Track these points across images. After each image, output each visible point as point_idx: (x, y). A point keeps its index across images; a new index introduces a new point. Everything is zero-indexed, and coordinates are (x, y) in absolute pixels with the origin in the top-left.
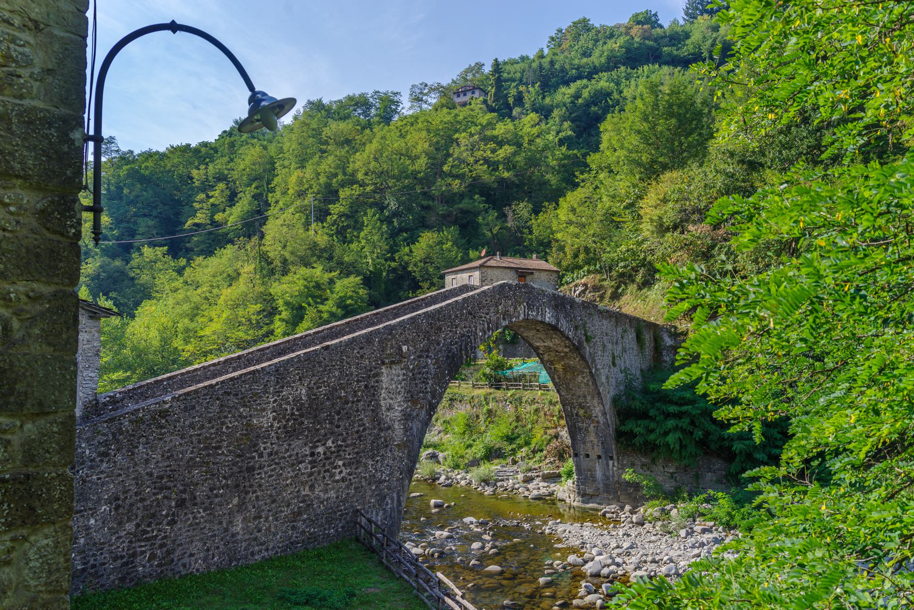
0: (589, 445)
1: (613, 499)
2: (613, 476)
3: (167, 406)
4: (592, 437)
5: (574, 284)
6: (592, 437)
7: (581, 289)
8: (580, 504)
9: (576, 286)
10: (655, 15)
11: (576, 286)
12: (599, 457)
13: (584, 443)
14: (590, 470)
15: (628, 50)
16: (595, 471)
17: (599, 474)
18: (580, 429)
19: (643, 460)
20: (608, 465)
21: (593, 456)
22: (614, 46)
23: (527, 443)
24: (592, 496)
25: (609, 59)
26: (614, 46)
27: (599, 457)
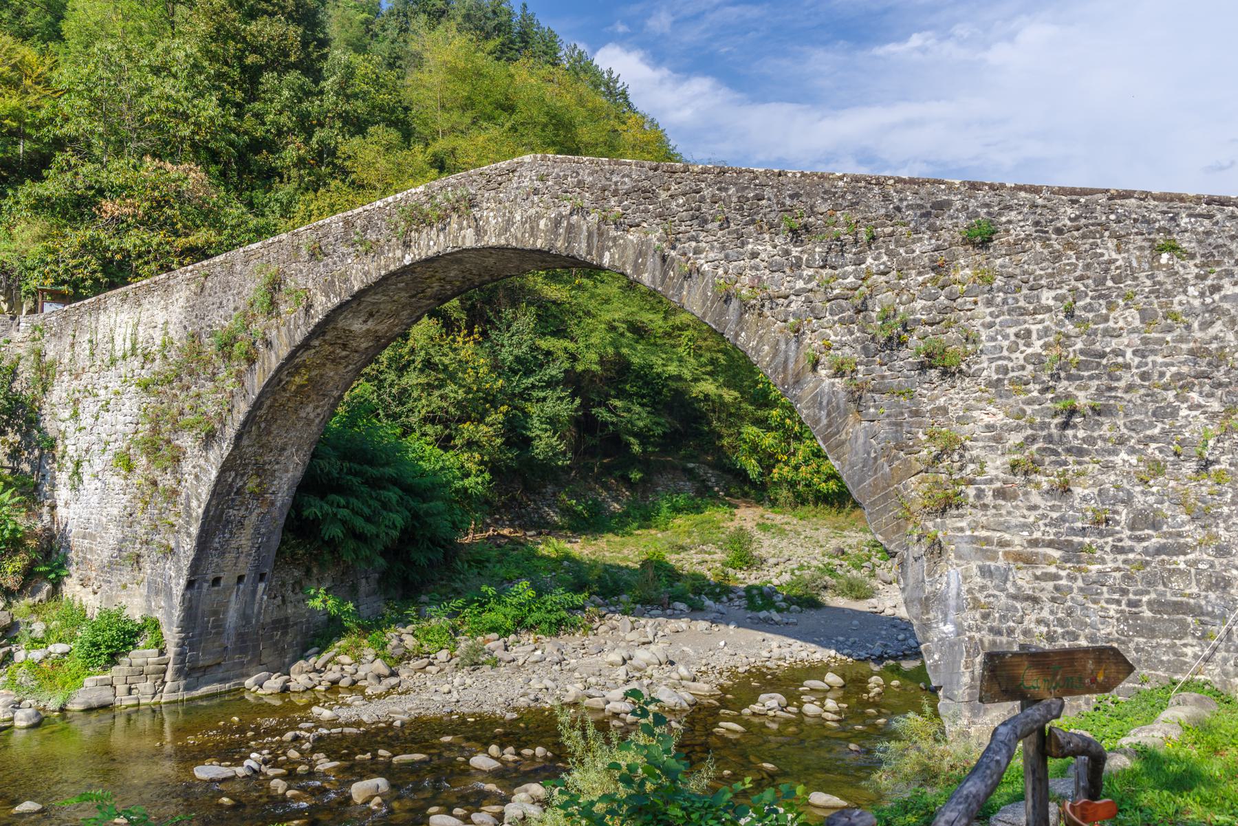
1: (250, 662)
3: (344, 353)
4: (244, 539)
6: (244, 539)
17: (232, 617)
20: (254, 592)
21: (228, 578)
24: (205, 669)
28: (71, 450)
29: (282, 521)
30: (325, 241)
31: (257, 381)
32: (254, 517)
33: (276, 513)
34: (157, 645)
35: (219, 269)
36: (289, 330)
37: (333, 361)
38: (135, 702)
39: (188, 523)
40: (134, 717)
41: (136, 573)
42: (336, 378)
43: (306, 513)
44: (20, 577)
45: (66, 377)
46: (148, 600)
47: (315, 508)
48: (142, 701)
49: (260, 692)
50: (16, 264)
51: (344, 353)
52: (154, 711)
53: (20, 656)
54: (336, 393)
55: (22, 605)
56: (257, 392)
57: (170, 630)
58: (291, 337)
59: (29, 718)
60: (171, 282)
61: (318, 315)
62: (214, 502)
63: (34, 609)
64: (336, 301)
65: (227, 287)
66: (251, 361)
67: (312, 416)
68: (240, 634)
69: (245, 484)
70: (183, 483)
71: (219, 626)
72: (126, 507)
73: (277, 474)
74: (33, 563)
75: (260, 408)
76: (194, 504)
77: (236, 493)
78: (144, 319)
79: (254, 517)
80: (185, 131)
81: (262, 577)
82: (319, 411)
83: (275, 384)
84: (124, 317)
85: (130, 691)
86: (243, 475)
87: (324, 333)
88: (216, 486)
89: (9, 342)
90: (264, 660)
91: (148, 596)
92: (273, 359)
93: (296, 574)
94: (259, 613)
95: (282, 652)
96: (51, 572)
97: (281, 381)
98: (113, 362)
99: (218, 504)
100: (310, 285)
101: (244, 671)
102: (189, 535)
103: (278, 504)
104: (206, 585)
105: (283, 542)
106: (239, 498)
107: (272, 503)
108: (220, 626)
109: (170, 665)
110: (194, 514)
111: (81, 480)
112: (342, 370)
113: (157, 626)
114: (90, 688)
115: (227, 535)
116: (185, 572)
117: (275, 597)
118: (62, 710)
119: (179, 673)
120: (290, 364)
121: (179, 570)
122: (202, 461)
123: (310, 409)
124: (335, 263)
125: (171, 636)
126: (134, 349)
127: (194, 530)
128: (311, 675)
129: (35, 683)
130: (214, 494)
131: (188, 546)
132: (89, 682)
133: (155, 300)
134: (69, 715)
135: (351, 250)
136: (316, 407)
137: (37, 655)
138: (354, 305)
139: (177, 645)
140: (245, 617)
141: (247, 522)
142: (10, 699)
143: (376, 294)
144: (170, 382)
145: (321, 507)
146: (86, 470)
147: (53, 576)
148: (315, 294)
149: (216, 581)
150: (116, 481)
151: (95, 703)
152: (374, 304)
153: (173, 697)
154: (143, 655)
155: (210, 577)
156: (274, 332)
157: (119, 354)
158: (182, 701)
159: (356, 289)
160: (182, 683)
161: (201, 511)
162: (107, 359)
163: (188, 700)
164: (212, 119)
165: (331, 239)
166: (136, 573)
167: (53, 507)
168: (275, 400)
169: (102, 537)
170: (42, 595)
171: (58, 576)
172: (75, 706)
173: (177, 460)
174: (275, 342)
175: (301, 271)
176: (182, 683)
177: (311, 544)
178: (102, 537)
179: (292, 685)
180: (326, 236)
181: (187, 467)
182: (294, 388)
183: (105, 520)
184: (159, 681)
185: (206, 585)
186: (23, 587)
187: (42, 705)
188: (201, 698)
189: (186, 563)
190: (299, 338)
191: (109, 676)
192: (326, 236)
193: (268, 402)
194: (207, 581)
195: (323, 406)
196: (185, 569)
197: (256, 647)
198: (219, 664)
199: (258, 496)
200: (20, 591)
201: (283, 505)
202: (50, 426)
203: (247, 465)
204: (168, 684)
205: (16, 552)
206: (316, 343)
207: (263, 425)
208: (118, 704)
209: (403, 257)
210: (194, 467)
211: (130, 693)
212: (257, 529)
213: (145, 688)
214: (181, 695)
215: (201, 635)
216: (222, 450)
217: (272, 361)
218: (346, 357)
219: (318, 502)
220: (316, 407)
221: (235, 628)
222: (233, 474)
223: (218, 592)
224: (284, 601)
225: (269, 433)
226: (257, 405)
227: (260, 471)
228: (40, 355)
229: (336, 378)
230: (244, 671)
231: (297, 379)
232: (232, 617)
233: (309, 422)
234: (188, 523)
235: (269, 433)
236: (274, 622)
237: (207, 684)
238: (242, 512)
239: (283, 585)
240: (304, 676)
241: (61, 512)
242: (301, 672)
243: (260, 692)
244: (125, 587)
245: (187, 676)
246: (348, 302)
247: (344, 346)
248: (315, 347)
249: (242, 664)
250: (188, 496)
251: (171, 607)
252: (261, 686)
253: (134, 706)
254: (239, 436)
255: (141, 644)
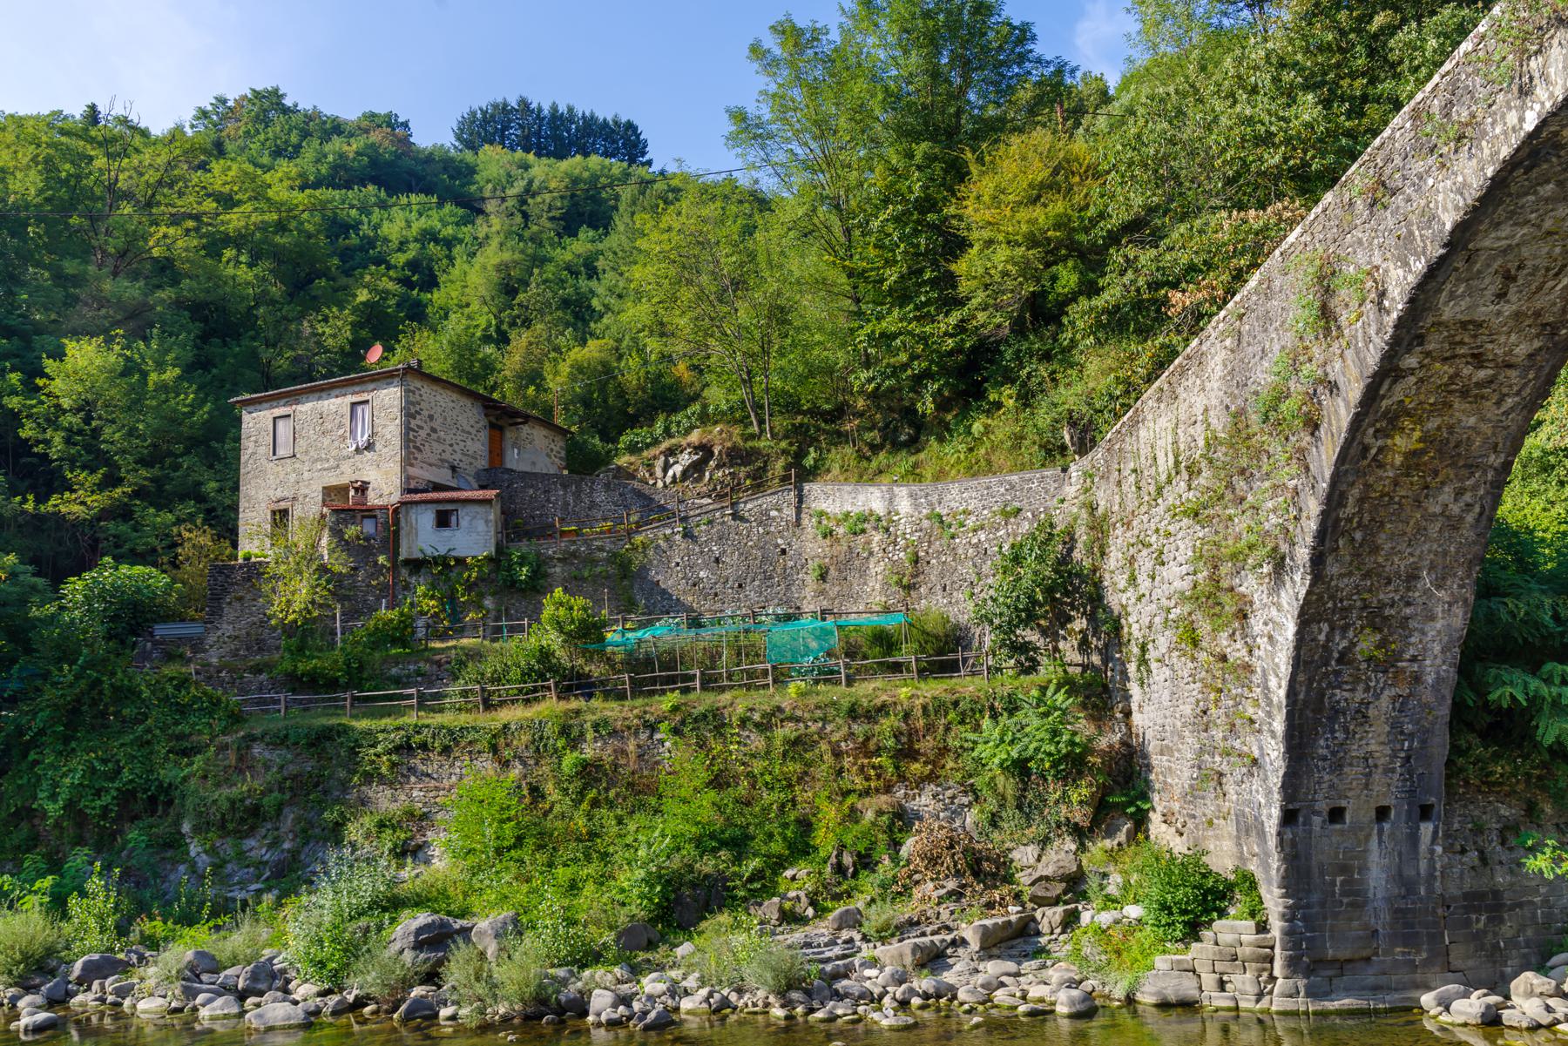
0: (1353, 772)
1: (1426, 963)
2: (1431, 876)
3: (1482, 374)
4: (1375, 741)
5: (665, 445)
6: (1375, 741)
7: (686, 459)
8: (1301, 1003)
9: (671, 452)
10: (405, 125)
11: (671, 452)
12: (1382, 813)
13: (1338, 767)
14: (1344, 869)
15: (374, 162)
16: (1363, 869)
17: (1377, 876)
18: (1336, 712)
19: (1504, 811)
20: (1414, 839)
21: (1358, 810)
22: (346, 148)
23: (801, 847)
24: (1341, 965)
25: (335, 168)
26: (346, 148)
27: (1382, 813)
28: (1136, 633)
29: (1444, 711)
30: (1388, 172)
31: (1325, 458)
32: (1385, 701)
33: (1428, 697)
34: (1253, 914)
35: (1254, 298)
36: (1358, 352)
37: (1464, 393)
38: (1231, 1004)
39: (1269, 714)
40: (1234, 1028)
41: (1220, 801)
42: (1486, 428)
43: (1493, 697)
44: (1089, 810)
45: (1119, 532)
46: (1239, 845)
47: (1511, 687)
48: (1242, 1005)
49: (1445, 1018)
50: (1084, 409)
51: (1482, 374)
52: (1260, 1021)
53: (1086, 917)
54: (1495, 460)
55: (1099, 847)
56: (1328, 474)
57: (1270, 892)
58: (1362, 362)
59: (1072, 1002)
60: (1204, 348)
61: (1397, 302)
62: (1301, 678)
63: (1112, 856)
64: (1419, 266)
65: (1267, 319)
66: (1313, 426)
67: (1455, 509)
68: (1397, 911)
69: (1353, 644)
70: (1256, 652)
71: (1356, 896)
72: (1198, 701)
73: (1412, 624)
74: (1105, 791)
75: (1341, 503)
76: (1273, 683)
77: (1340, 661)
78: (1183, 417)
79: (1385, 701)
80: (1273, 159)
81: (1425, 813)
82: (1467, 497)
83: (1353, 455)
84: (1163, 422)
85: (1222, 985)
86: (1345, 629)
87: (1421, 339)
88: (1298, 648)
89: (1062, 501)
90: (1456, 963)
91: (1238, 838)
92: (1343, 411)
93: (1504, 811)
94: (1431, 876)
95: (1495, 955)
96: (1131, 803)
97: (1366, 449)
98: (1160, 491)
99: (1310, 681)
100: (1377, 260)
101: (1418, 977)
102: (1273, 734)
103: (1430, 679)
104: (1317, 820)
105: (1456, 750)
106: (1347, 672)
107: (1417, 679)
108: (1357, 893)
109: (1277, 950)
110: (1275, 699)
111: (1149, 671)
112: (1490, 410)
113: (1253, 886)
114: (1161, 974)
115: (1340, 735)
116: (1276, 796)
117: (1463, 851)
118: (1130, 1000)
119: (1293, 965)
120: (1374, 408)
121: (1269, 792)
122: (1274, 612)
123: (1447, 494)
124: (1409, 200)
125: (1274, 901)
126: (1177, 463)
127: (1279, 725)
128: (1552, 1002)
129: (1103, 957)
130: (1298, 662)
131: (1274, 753)
132: (1161, 962)
133: (1190, 383)
134: (1140, 1008)
135: (1430, 161)
136: (1459, 493)
137: (1105, 918)
138: (1460, 264)
139: (1283, 916)
140: (1405, 884)
141: (1372, 712)
142: (1067, 975)
143: (1497, 225)
144: (1221, 497)
145: (1526, 685)
146: (1152, 655)
147: (1131, 810)
148: (1386, 271)
149: (1336, 815)
150: (1185, 668)
151: (1172, 998)
152: (1505, 251)
153: (1289, 1004)
154: (1233, 929)
155: (1323, 806)
156: (1338, 365)
157: (1163, 478)
158: (1306, 1013)
159: (1448, 227)
160: (1301, 983)
161: (1282, 693)
162: (1152, 489)
163: (1316, 1013)
164: (1309, 126)
165: (1398, 160)
166: (1220, 801)
167: (1128, 714)
168: (1367, 486)
169: (1179, 750)
170: (1122, 836)
171: (1139, 810)
172: (1146, 998)
173: (1243, 616)
174: (1341, 381)
175: (1360, 242)
176: (1301, 983)
177: (1526, 757)
178: (1179, 750)
179: (1506, 1015)
180: (1389, 160)
181: (1257, 625)
182: (1398, 460)
183: (1179, 724)
184: (1265, 975)
185: (1317, 820)
186: (1096, 822)
187: (1107, 990)
188: (1339, 1013)
189: (1276, 780)
190: (1373, 359)
191: (1189, 957)
192: (1389, 160)
193: (1355, 492)
194: (1318, 813)
195: (1475, 488)
196: (1275, 789)
197: (1435, 938)
198: (1368, 959)
199: (1386, 664)
200: (1091, 830)
201: (1439, 680)
202: (1114, 600)
203: (1351, 608)
204: (1280, 981)
205: (1080, 774)
206: (1411, 361)
207: (1358, 536)
208: (1206, 1002)
209: (1522, 120)
210: (1266, 624)
211: (1223, 990)
212: (1396, 726)
213: (1243, 982)
214: (1301, 1003)
215: (1323, 904)
216: (1298, 585)
217: (1340, 414)
218: (1490, 381)
219: (1518, 676)
220: (1459, 493)
221: (1388, 900)
222: (1325, 627)
223: (1342, 832)
224: (1483, 859)
225: (1376, 549)
226: (1334, 500)
227: (1376, 619)
228: (1092, 509)
229: (1486, 428)
230: (1418, 977)
231: (1400, 442)
232: (1377, 876)
233: (1454, 524)
234: (1269, 714)
235: (1376, 549)
236: (1466, 896)
237: (1348, 991)
238: (1359, 695)
239: (1479, 830)
240: (1536, 1001)
241: (1137, 718)
242: (1530, 994)
243: (1445, 1018)
244: (1210, 823)
245: (1308, 972)
246: (1442, 258)
247: (1478, 359)
248: (1412, 371)
249: (1413, 966)
250: (1264, 671)
251: (1267, 855)
252: (1447, 1009)
253: (1229, 1009)
254: (1317, 561)
255: (1232, 911)
